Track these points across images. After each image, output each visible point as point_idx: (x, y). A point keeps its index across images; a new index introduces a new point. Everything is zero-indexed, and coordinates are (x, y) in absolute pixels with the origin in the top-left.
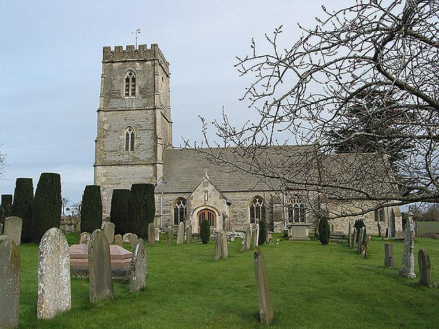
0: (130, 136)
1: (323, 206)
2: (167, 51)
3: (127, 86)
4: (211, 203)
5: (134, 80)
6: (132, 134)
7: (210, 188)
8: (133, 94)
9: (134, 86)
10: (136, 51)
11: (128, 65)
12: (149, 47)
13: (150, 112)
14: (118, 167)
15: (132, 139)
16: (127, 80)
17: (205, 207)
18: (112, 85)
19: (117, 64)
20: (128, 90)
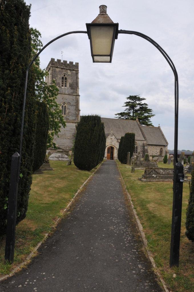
1: (146, 148)
3: (63, 81)
5: (66, 78)
6: (65, 107)
8: (66, 86)
9: (66, 82)
11: (64, 70)
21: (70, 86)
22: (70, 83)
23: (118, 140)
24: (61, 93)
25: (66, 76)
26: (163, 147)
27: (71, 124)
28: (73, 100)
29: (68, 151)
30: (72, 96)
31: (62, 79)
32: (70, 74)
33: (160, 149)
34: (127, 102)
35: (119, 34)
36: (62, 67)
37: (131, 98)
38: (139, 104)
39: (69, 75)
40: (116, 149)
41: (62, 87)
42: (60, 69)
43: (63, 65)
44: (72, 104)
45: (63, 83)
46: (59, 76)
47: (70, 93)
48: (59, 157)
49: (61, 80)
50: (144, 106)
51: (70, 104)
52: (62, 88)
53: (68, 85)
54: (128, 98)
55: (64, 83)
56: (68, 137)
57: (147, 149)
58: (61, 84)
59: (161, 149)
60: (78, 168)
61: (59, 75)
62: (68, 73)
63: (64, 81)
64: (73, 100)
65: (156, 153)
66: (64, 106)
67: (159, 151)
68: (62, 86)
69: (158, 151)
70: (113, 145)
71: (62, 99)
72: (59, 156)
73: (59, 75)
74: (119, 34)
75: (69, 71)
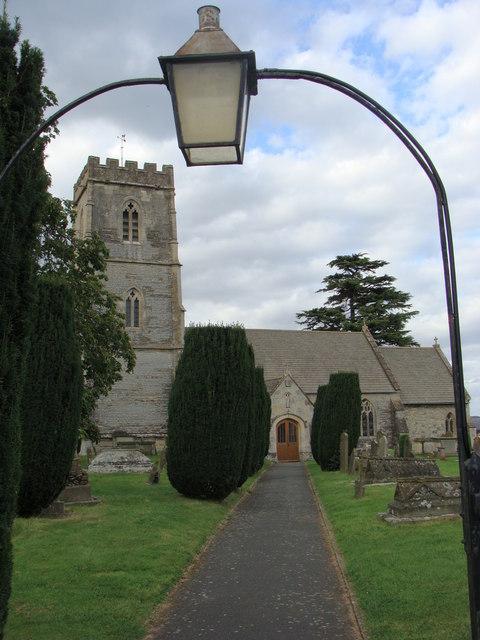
0: (133, 304)
1: (400, 415)
2: (113, 156)
3: (125, 224)
4: (294, 410)
5: (135, 215)
6: (137, 301)
7: (293, 389)
8: (135, 238)
9: (136, 224)
10: (140, 172)
11: (128, 191)
12: (159, 169)
13: (165, 269)
14: (374, 357)
15: (137, 308)
16: (126, 214)
17: (287, 417)
18: (104, 221)
19: (111, 187)
20: (126, 230)
21: (149, 237)
25: (135, 205)
28: (161, 279)
32: (148, 200)
33: (444, 417)
37: (340, 262)
39: (143, 204)
45: (126, 230)
49: (120, 221)
53: (142, 234)
56: (151, 398)
61: (113, 206)
63: (131, 221)
67: (444, 422)
68: (126, 237)
71: (127, 277)
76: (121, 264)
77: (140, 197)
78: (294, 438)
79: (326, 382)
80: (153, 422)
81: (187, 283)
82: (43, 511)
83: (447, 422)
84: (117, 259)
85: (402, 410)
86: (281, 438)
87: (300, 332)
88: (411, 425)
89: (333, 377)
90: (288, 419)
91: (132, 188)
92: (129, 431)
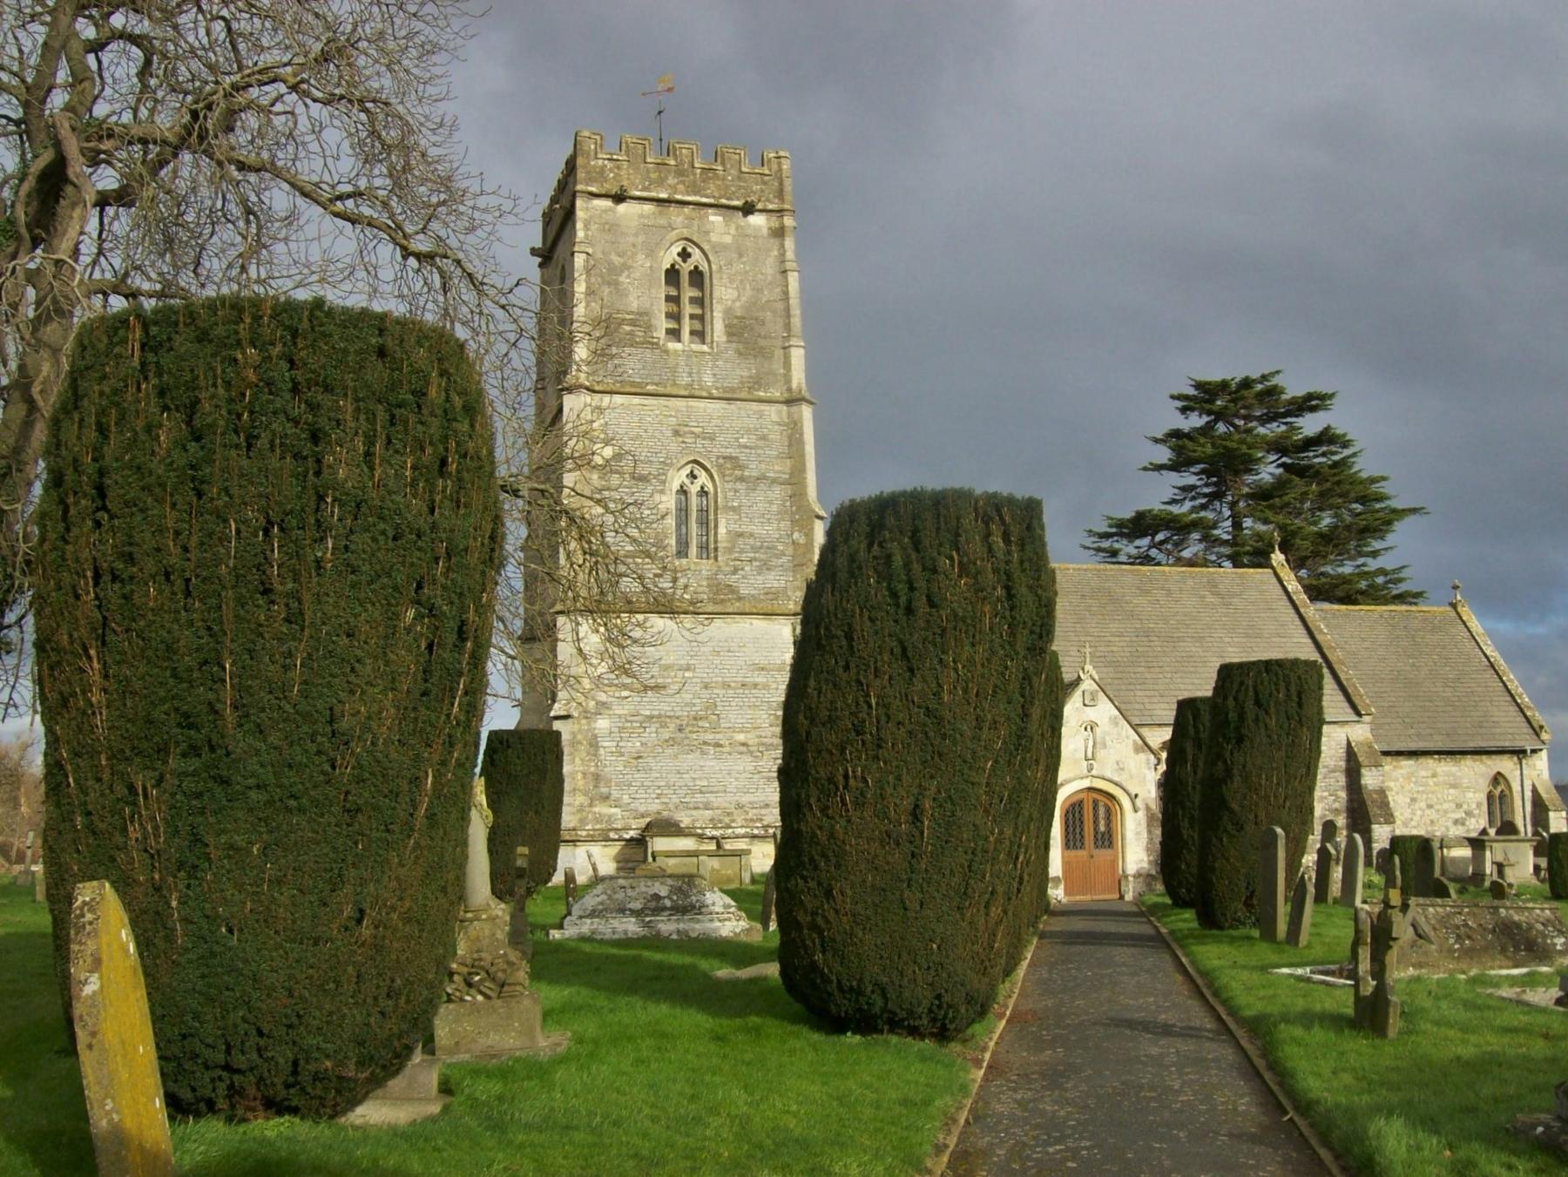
1: (1369, 779)
3: (673, 300)
5: (697, 277)
8: (699, 335)
9: (699, 302)
11: (677, 216)
21: (732, 332)
22: (728, 312)
23: (1145, 731)
24: (661, 390)
25: (696, 255)
26: (1507, 765)
27: (759, 624)
29: (741, 845)
30: (754, 406)
31: (668, 282)
32: (728, 239)
33: (1484, 786)
34: (1176, 434)
35: (1209, 694)
36: (663, 195)
37: (1205, 396)
38: (1279, 447)
39: (720, 248)
40: (1136, 811)
41: (673, 346)
42: (648, 208)
43: (671, 181)
44: (753, 471)
45: (675, 316)
46: (642, 262)
47: (735, 383)
48: (658, 910)
49: (662, 290)
50: (1316, 458)
51: (742, 468)
52: (667, 352)
54: (1188, 405)
55: (688, 309)
56: (741, 737)
57: (1382, 792)
58: (662, 324)
59: (1498, 778)
60: (798, 1007)
61: (640, 257)
62: (714, 238)
63: (689, 292)
64: (764, 438)
65: (1460, 815)
66: (694, 489)
67: (1482, 797)
69: (1476, 797)
70: (1108, 775)
71: (676, 433)
72: (656, 897)
73: (640, 257)
74: (1209, 694)
75: (715, 218)
76: (662, 401)
77: (707, 233)
78: (1107, 839)
79: (1203, 686)
80: (745, 799)
81: (779, 693)
82: (380, 1092)
83: (1490, 797)
84: (650, 388)
85: (1378, 765)
86: (1073, 839)
87: (143, 943)
88: (1397, 801)
89: (1227, 673)
90: (1090, 789)
91: (686, 210)
92: (685, 821)
